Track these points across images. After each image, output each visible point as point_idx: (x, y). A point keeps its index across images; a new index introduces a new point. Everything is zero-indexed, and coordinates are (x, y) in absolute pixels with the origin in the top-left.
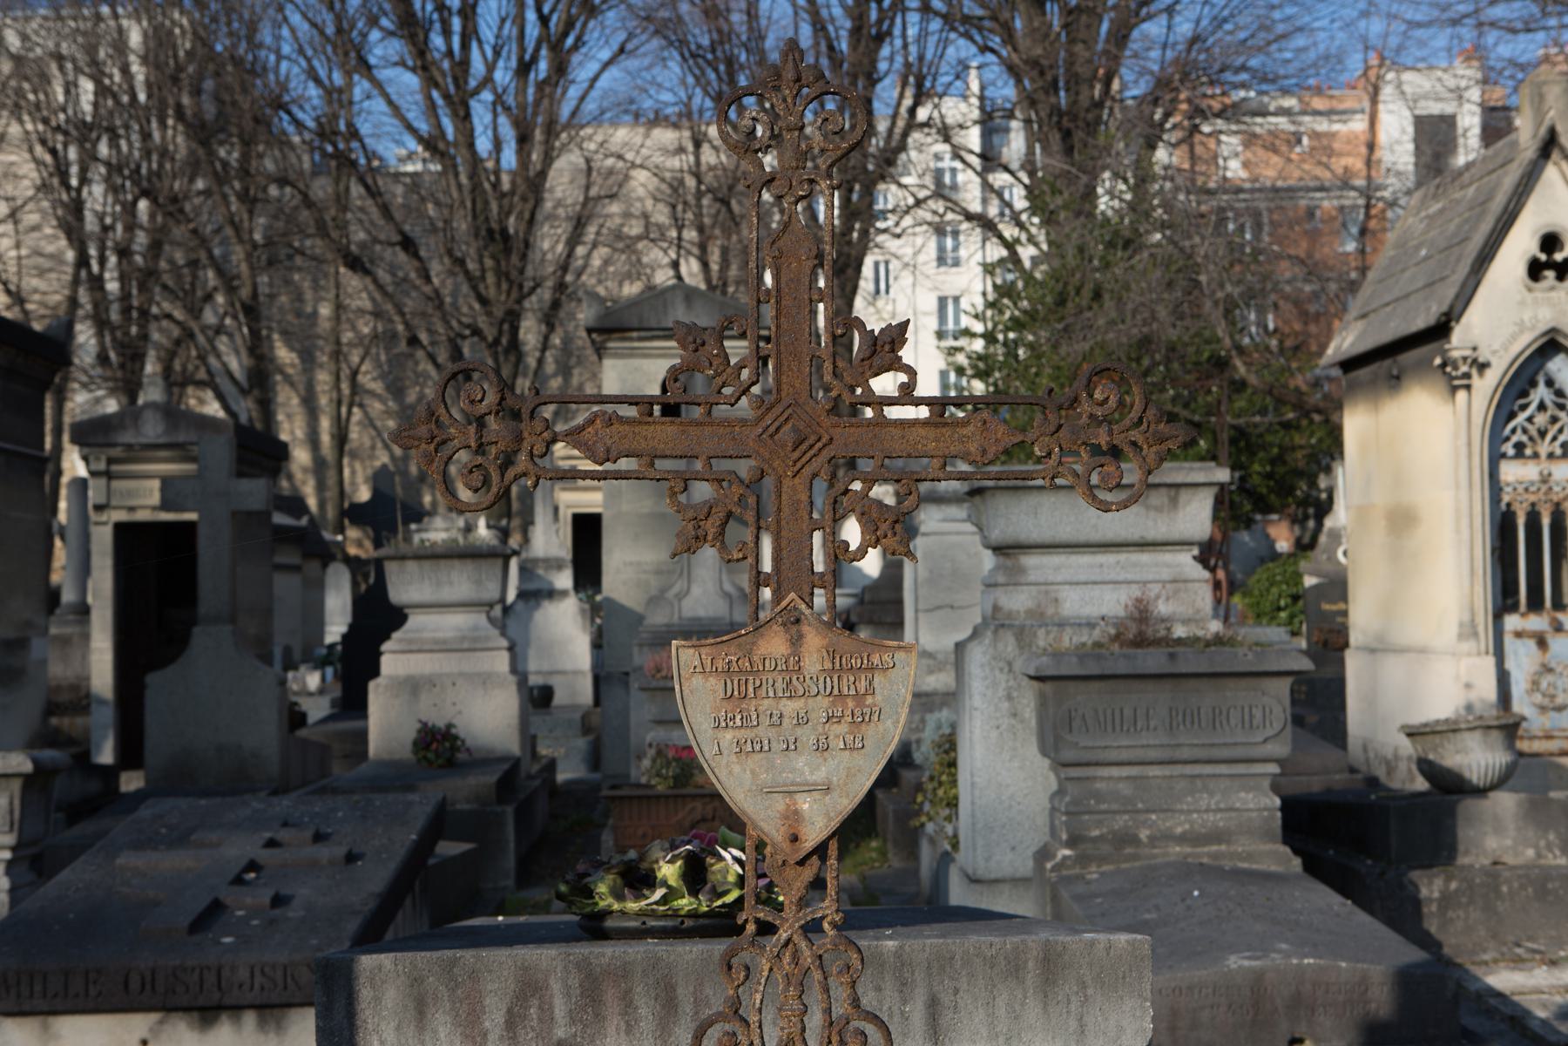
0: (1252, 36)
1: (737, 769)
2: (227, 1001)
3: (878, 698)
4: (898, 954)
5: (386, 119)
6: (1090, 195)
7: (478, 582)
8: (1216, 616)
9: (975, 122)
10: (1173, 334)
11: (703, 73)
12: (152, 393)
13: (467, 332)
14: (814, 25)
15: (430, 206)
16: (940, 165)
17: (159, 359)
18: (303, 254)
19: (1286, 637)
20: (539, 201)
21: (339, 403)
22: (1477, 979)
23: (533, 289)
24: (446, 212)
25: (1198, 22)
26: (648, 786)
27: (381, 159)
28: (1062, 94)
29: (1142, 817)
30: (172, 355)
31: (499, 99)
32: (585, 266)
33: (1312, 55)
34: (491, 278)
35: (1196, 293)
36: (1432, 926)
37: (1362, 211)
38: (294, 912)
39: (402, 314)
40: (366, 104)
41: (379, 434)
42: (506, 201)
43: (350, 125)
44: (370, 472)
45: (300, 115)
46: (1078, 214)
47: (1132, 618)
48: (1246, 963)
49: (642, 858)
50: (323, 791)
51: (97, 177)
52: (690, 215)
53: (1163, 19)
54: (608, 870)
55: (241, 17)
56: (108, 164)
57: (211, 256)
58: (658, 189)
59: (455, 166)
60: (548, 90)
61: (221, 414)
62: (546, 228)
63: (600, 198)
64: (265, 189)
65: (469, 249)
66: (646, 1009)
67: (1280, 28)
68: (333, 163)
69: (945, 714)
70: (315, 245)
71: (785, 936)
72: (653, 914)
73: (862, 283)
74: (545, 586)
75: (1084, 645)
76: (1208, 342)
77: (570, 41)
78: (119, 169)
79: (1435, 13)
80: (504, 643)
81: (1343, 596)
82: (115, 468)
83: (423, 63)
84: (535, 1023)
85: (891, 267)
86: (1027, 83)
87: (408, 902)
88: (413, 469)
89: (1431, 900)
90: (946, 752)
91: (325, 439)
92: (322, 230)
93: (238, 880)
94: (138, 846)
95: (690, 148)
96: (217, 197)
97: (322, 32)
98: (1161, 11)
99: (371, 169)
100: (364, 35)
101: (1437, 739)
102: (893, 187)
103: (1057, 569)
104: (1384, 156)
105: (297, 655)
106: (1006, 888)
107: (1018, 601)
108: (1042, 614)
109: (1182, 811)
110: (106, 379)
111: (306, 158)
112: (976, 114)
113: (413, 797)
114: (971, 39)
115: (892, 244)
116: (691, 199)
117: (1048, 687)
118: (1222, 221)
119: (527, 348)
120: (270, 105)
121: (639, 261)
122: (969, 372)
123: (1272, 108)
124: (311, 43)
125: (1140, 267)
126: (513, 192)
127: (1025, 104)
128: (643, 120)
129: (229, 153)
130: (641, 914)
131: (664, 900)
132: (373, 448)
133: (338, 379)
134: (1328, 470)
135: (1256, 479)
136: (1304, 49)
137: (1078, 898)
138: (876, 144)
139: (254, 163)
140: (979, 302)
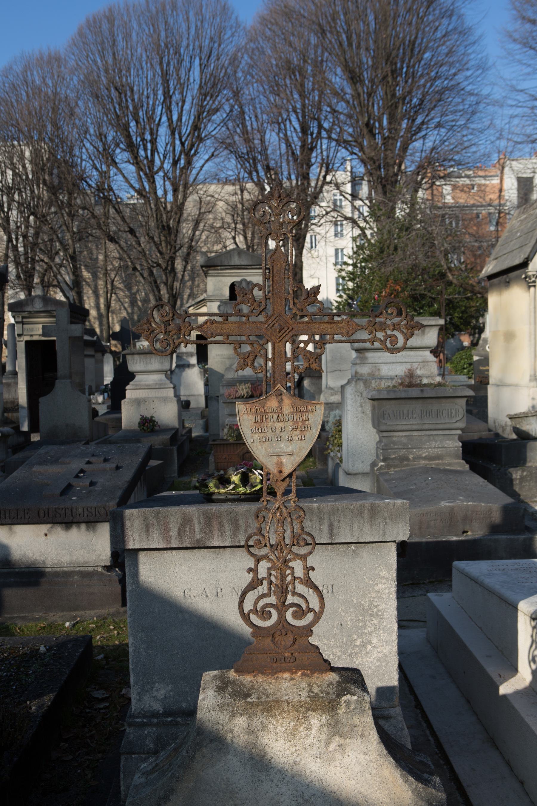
0: (456, 147)
1: (260, 447)
2: (75, 520)
3: (310, 422)
4: (318, 508)
5: (123, 183)
6: (393, 209)
7: (162, 363)
8: (439, 375)
9: (349, 182)
10: (424, 264)
11: (244, 164)
12: (37, 292)
13: (155, 265)
14: (286, 144)
15: (140, 217)
16: (335, 198)
17: (39, 277)
18: (92, 236)
19: (467, 379)
20: (181, 214)
21: (107, 293)
22: (532, 507)
23: (180, 248)
24: (146, 219)
25: (435, 141)
26: (226, 440)
27: (121, 198)
28: (382, 170)
29: (410, 450)
30: (44, 275)
31: (166, 175)
32: (200, 239)
33: (478, 154)
34: (164, 244)
35: (434, 248)
36: (517, 489)
37: (497, 215)
38: (98, 488)
39: (130, 258)
40: (115, 177)
41: (122, 304)
42: (169, 214)
43: (109, 186)
44: (119, 318)
45: (90, 182)
46: (389, 218)
47: (406, 376)
48: (447, 504)
49: (226, 473)
50: (105, 442)
51: (14, 208)
52: (239, 219)
53: (421, 141)
54: (213, 478)
55: (67, 145)
56: (18, 202)
57: (58, 237)
58: (227, 209)
59: (149, 201)
60: (184, 171)
61: (63, 299)
62: (184, 225)
63: (205, 212)
64: (77, 211)
65: (155, 233)
66: (228, 528)
67: (466, 144)
68: (103, 201)
69: (337, 412)
70: (97, 232)
71: (277, 506)
72: (230, 494)
73: (306, 244)
74: (186, 363)
75: (389, 386)
76: (438, 267)
77: (193, 152)
78: (23, 205)
79: (525, 138)
80: (172, 386)
81: (488, 365)
82: (24, 320)
83: (136, 161)
84: (188, 533)
85: (317, 238)
86: (369, 167)
87: (139, 484)
88: (136, 317)
89: (516, 479)
90: (338, 426)
91: (102, 306)
92: (99, 227)
93: (77, 476)
94: (40, 463)
95: (239, 192)
96: (59, 215)
97: (98, 150)
98: (420, 138)
99: (118, 203)
100: (114, 151)
101: (520, 420)
102: (317, 207)
103: (379, 358)
104: (506, 195)
105: (94, 389)
106: (360, 476)
107: (364, 370)
108: (373, 375)
109: (425, 448)
110: (20, 285)
111: (92, 199)
112: (349, 178)
113: (140, 445)
114: (347, 149)
115: (317, 229)
116: (240, 213)
117: (376, 403)
118: (443, 220)
119: (177, 271)
120: (79, 179)
121: (220, 236)
122: (347, 279)
123: (463, 175)
124: (94, 154)
125: (412, 238)
126: (171, 211)
127: (368, 174)
128: (221, 182)
129: (63, 197)
130: (226, 493)
131: (234, 489)
132: (120, 309)
133: (106, 284)
134: (483, 316)
135: (456, 319)
136: (475, 152)
137: (386, 481)
138: (311, 190)
139: (73, 201)
140: (351, 253)
